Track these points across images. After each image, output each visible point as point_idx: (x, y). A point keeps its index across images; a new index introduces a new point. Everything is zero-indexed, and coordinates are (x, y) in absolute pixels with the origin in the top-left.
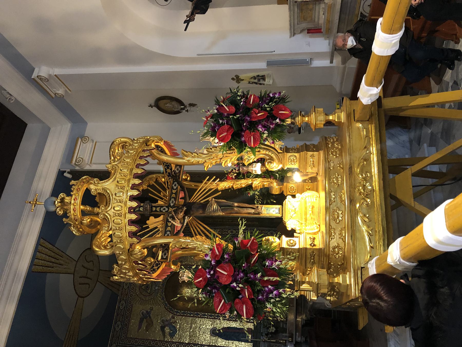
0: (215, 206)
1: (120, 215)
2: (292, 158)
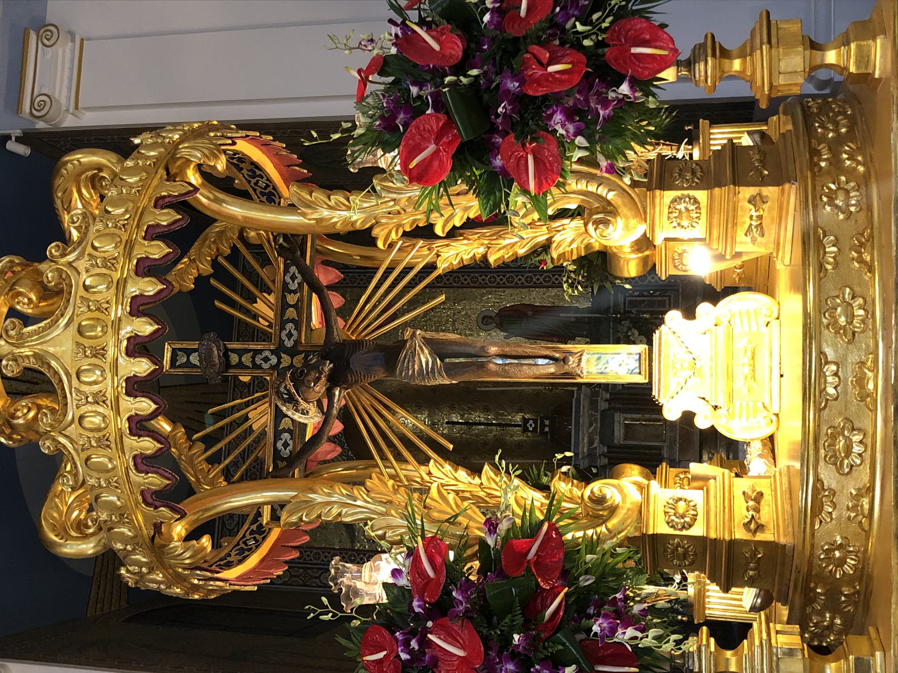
0: (425, 357)
1: (103, 443)
2: (682, 206)
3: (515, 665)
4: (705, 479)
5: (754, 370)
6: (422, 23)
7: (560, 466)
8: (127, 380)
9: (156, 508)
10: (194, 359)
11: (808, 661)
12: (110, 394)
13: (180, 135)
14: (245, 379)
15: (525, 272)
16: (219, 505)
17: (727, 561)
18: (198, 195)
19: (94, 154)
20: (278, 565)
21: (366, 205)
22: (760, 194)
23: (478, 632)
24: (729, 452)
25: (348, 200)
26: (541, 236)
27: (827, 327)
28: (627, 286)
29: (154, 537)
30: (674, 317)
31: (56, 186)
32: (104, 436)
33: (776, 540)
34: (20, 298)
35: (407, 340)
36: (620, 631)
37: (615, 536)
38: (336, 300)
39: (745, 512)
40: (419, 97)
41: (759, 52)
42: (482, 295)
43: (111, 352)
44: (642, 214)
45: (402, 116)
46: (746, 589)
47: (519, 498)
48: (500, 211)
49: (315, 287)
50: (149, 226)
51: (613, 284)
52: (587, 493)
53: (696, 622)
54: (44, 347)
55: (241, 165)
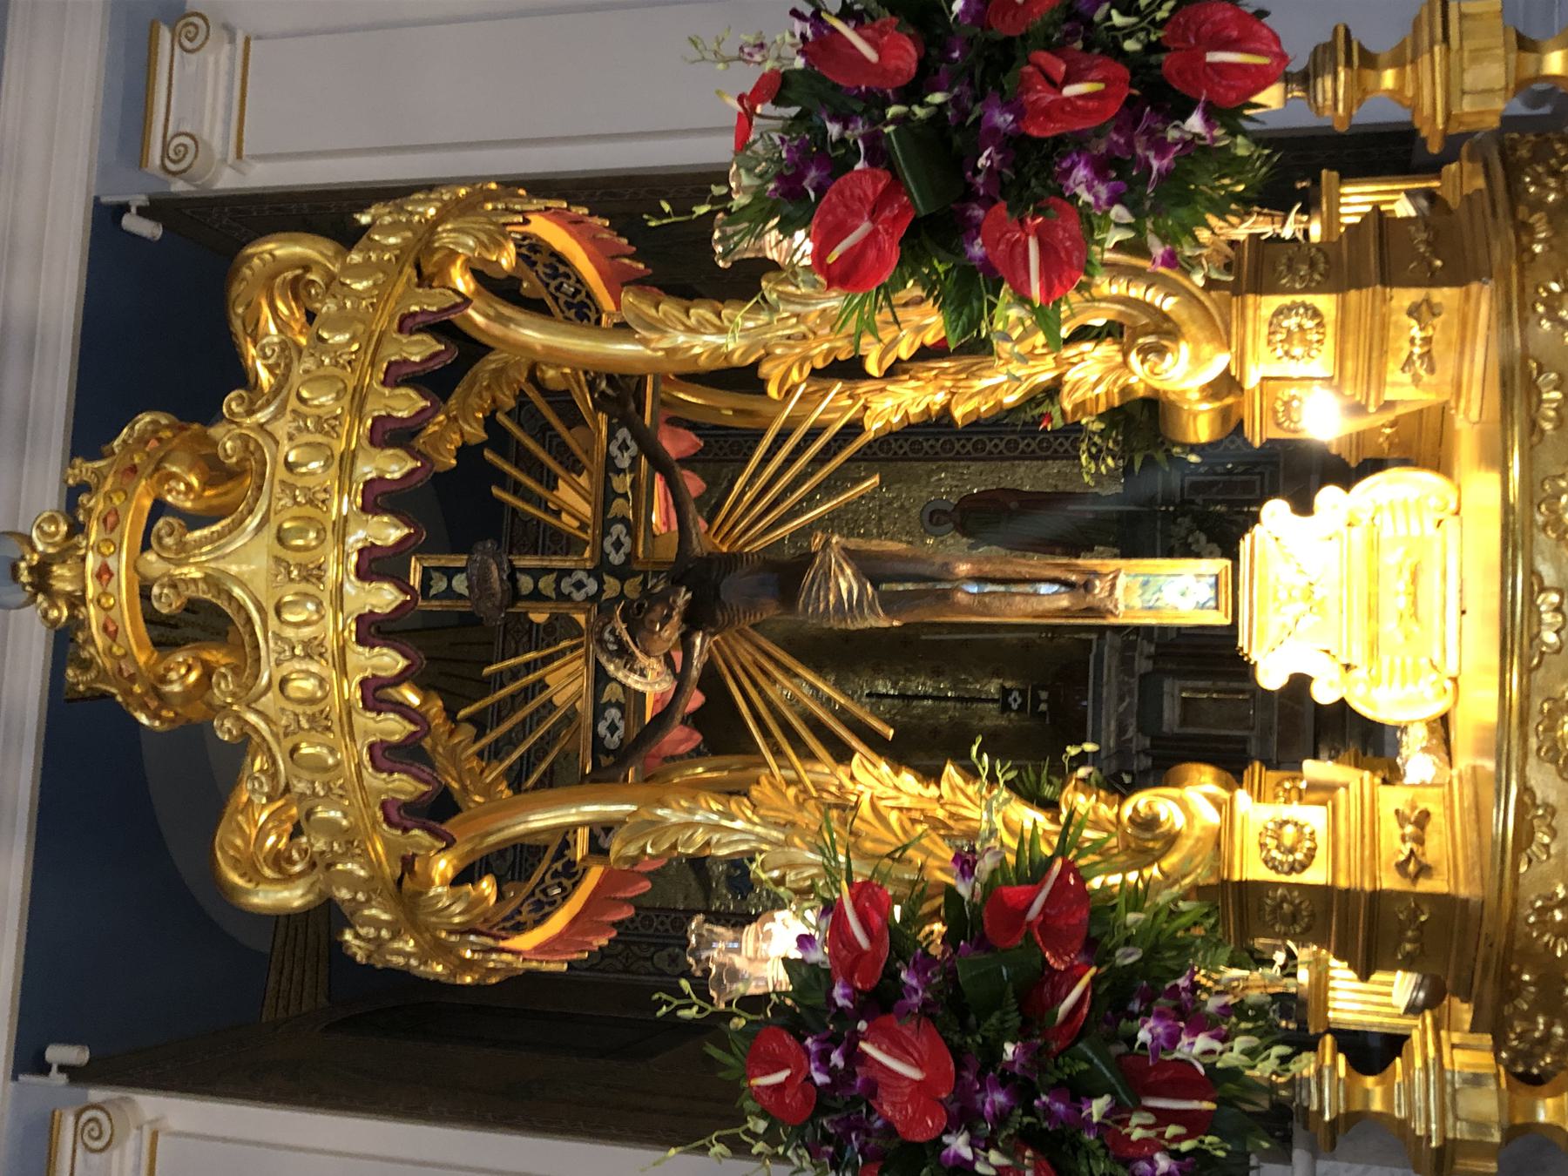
0: (846, 582)
1: (321, 723)
2: (1291, 322)
3: (1007, 1094)
4: (1330, 788)
5: (1415, 603)
6: (845, 14)
7: (1074, 769)
8: (360, 619)
9: (406, 830)
10: (460, 584)
11: (1507, 1095)
12: (331, 643)
13: (438, 210)
14: (539, 617)
15: (1006, 433)
16: (508, 827)
17: (1365, 926)
18: (470, 312)
19: (297, 242)
20: (599, 930)
21: (750, 324)
22: (1427, 301)
23: (946, 1040)
24: (1370, 743)
25: (719, 315)
26: (1044, 372)
27: (1544, 529)
28: (1193, 458)
29: (400, 882)
30: (1275, 511)
31: (233, 294)
32: (322, 712)
33: (1453, 891)
34: (173, 483)
35: (815, 554)
36: (1185, 1040)
37: (1176, 882)
38: (694, 484)
39: (1398, 843)
40: (842, 141)
41: (1427, 57)
42: (930, 473)
43: (332, 572)
44: (1223, 334)
45: (813, 173)
46: (1400, 973)
47: (1009, 820)
48: (979, 332)
49: (660, 463)
50: (390, 364)
51: (1170, 456)
52: (1127, 811)
53: (1312, 1031)
54: (221, 565)
55: (534, 257)
